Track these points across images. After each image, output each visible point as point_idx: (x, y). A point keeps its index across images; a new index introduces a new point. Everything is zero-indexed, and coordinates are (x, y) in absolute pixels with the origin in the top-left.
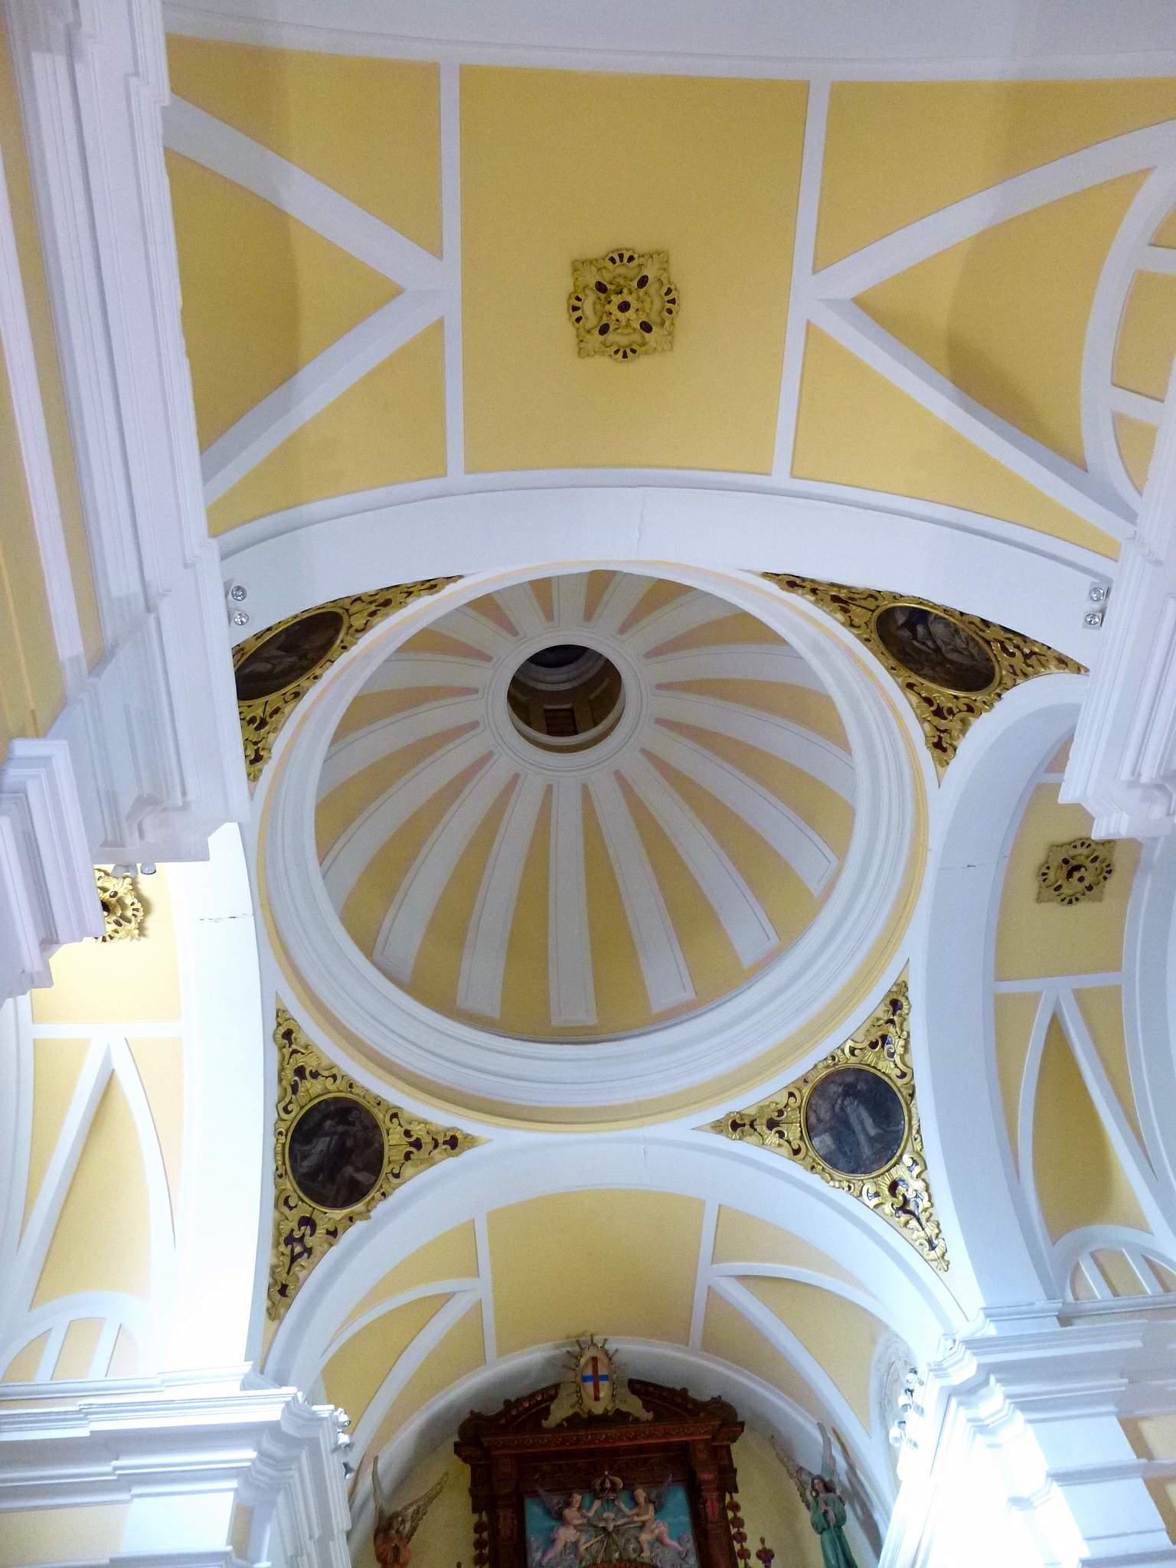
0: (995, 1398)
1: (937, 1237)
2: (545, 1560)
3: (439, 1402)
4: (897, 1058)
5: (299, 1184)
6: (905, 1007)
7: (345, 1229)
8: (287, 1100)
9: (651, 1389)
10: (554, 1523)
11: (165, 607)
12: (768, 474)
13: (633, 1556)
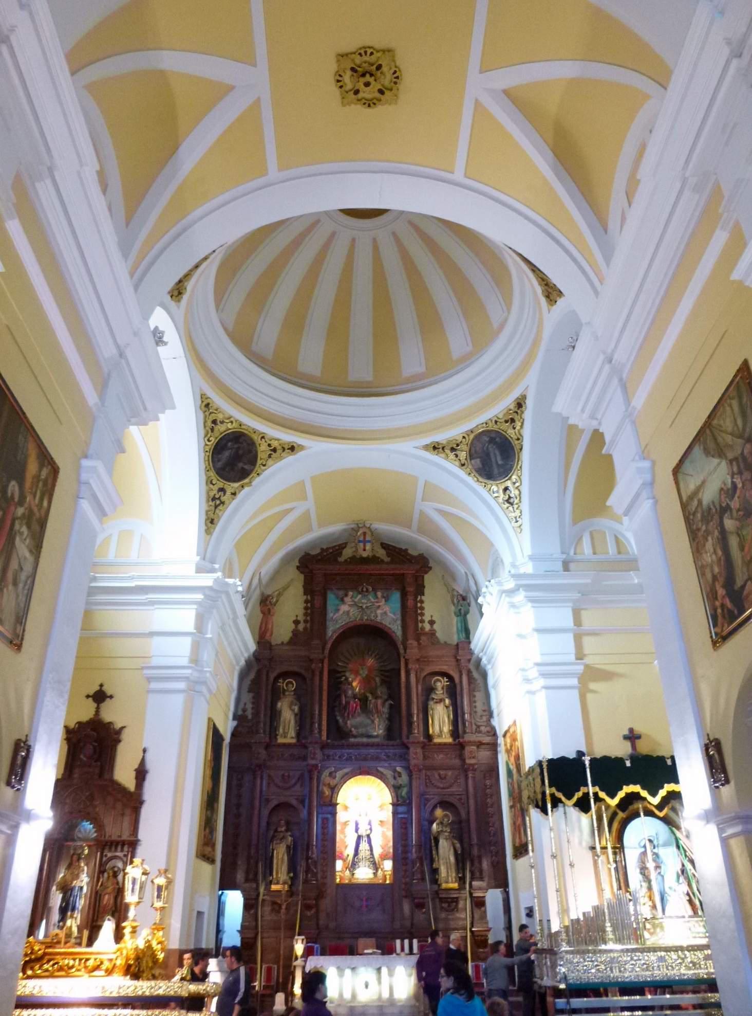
0: (521, 596)
1: (519, 517)
2: (335, 616)
3: (291, 546)
4: (516, 430)
6: (524, 407)
7: (240, 491)
8: (209, 435)
9: (391, 548)
11: (129, 353)
12: (452, 173)
13: (373, 618)
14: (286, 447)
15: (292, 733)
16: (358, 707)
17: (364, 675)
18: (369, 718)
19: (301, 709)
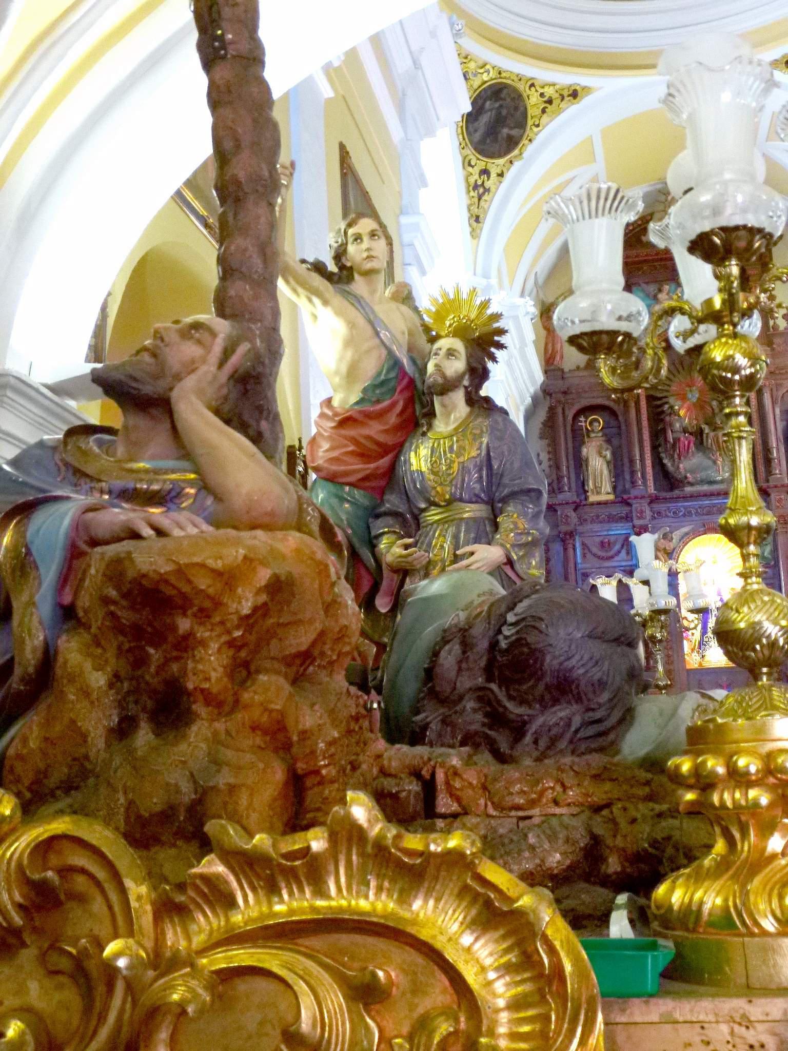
5: (475, 149)
7: (508, 170)
10: (653, 302)
11: (424, 61)
14: (566, 93)
15: (607, 487)
16: (692, 445)
17: (694, 400)
18: (710, 458)
19: (614, 454)
